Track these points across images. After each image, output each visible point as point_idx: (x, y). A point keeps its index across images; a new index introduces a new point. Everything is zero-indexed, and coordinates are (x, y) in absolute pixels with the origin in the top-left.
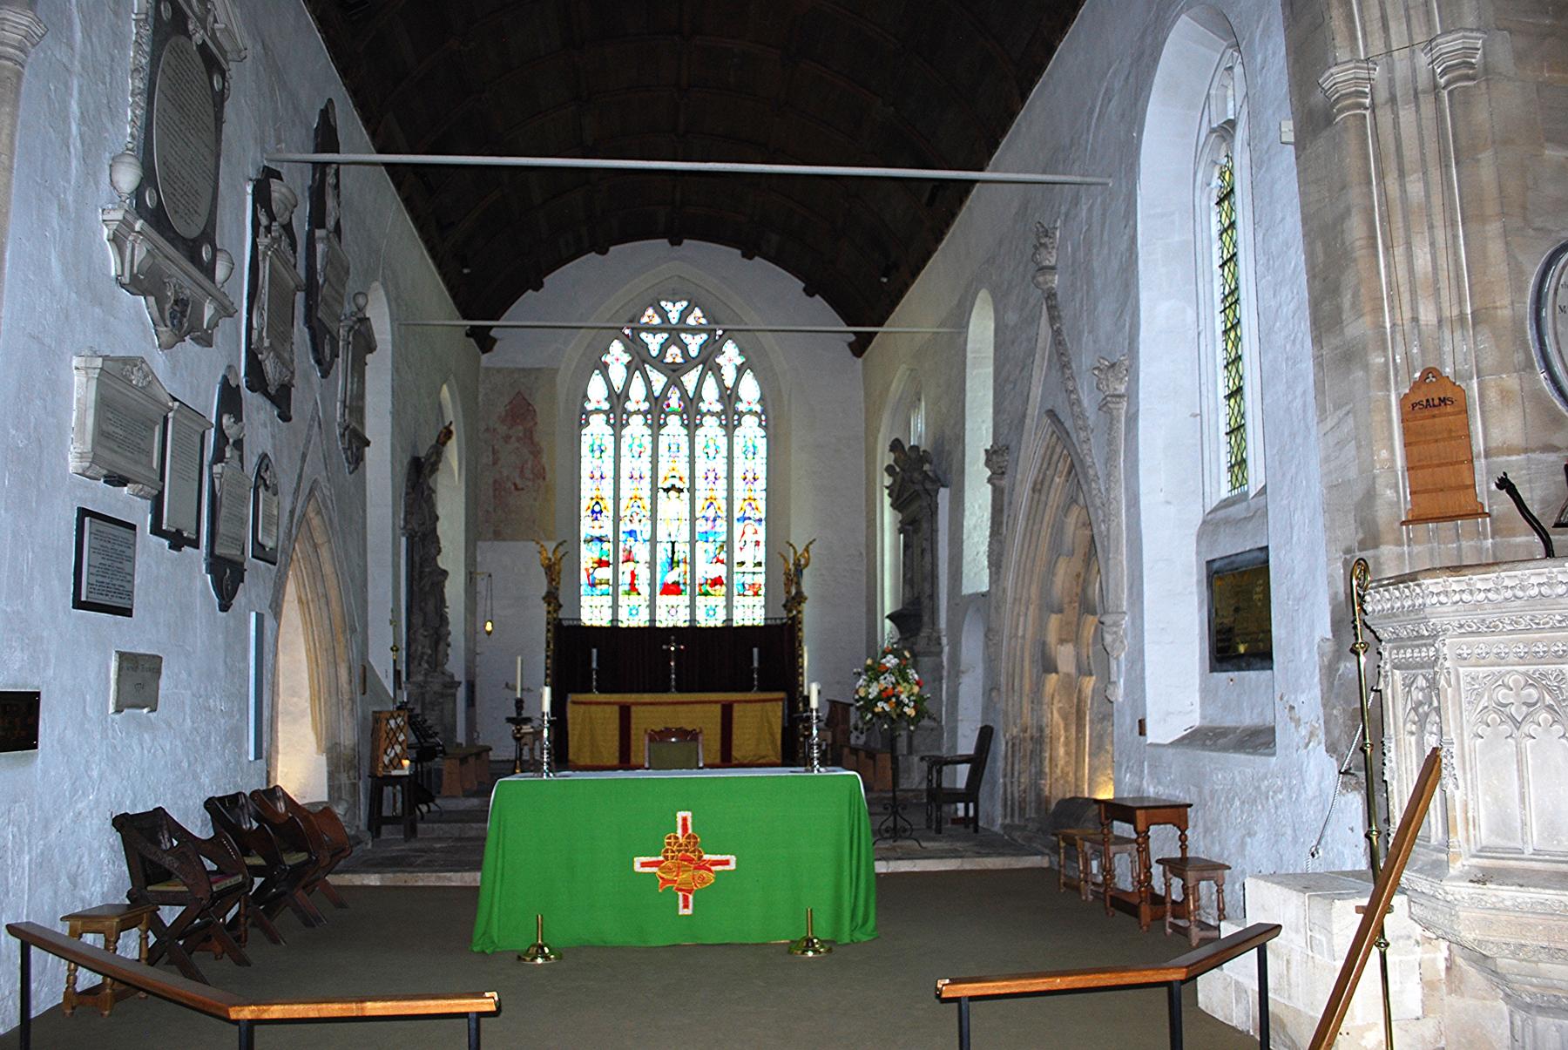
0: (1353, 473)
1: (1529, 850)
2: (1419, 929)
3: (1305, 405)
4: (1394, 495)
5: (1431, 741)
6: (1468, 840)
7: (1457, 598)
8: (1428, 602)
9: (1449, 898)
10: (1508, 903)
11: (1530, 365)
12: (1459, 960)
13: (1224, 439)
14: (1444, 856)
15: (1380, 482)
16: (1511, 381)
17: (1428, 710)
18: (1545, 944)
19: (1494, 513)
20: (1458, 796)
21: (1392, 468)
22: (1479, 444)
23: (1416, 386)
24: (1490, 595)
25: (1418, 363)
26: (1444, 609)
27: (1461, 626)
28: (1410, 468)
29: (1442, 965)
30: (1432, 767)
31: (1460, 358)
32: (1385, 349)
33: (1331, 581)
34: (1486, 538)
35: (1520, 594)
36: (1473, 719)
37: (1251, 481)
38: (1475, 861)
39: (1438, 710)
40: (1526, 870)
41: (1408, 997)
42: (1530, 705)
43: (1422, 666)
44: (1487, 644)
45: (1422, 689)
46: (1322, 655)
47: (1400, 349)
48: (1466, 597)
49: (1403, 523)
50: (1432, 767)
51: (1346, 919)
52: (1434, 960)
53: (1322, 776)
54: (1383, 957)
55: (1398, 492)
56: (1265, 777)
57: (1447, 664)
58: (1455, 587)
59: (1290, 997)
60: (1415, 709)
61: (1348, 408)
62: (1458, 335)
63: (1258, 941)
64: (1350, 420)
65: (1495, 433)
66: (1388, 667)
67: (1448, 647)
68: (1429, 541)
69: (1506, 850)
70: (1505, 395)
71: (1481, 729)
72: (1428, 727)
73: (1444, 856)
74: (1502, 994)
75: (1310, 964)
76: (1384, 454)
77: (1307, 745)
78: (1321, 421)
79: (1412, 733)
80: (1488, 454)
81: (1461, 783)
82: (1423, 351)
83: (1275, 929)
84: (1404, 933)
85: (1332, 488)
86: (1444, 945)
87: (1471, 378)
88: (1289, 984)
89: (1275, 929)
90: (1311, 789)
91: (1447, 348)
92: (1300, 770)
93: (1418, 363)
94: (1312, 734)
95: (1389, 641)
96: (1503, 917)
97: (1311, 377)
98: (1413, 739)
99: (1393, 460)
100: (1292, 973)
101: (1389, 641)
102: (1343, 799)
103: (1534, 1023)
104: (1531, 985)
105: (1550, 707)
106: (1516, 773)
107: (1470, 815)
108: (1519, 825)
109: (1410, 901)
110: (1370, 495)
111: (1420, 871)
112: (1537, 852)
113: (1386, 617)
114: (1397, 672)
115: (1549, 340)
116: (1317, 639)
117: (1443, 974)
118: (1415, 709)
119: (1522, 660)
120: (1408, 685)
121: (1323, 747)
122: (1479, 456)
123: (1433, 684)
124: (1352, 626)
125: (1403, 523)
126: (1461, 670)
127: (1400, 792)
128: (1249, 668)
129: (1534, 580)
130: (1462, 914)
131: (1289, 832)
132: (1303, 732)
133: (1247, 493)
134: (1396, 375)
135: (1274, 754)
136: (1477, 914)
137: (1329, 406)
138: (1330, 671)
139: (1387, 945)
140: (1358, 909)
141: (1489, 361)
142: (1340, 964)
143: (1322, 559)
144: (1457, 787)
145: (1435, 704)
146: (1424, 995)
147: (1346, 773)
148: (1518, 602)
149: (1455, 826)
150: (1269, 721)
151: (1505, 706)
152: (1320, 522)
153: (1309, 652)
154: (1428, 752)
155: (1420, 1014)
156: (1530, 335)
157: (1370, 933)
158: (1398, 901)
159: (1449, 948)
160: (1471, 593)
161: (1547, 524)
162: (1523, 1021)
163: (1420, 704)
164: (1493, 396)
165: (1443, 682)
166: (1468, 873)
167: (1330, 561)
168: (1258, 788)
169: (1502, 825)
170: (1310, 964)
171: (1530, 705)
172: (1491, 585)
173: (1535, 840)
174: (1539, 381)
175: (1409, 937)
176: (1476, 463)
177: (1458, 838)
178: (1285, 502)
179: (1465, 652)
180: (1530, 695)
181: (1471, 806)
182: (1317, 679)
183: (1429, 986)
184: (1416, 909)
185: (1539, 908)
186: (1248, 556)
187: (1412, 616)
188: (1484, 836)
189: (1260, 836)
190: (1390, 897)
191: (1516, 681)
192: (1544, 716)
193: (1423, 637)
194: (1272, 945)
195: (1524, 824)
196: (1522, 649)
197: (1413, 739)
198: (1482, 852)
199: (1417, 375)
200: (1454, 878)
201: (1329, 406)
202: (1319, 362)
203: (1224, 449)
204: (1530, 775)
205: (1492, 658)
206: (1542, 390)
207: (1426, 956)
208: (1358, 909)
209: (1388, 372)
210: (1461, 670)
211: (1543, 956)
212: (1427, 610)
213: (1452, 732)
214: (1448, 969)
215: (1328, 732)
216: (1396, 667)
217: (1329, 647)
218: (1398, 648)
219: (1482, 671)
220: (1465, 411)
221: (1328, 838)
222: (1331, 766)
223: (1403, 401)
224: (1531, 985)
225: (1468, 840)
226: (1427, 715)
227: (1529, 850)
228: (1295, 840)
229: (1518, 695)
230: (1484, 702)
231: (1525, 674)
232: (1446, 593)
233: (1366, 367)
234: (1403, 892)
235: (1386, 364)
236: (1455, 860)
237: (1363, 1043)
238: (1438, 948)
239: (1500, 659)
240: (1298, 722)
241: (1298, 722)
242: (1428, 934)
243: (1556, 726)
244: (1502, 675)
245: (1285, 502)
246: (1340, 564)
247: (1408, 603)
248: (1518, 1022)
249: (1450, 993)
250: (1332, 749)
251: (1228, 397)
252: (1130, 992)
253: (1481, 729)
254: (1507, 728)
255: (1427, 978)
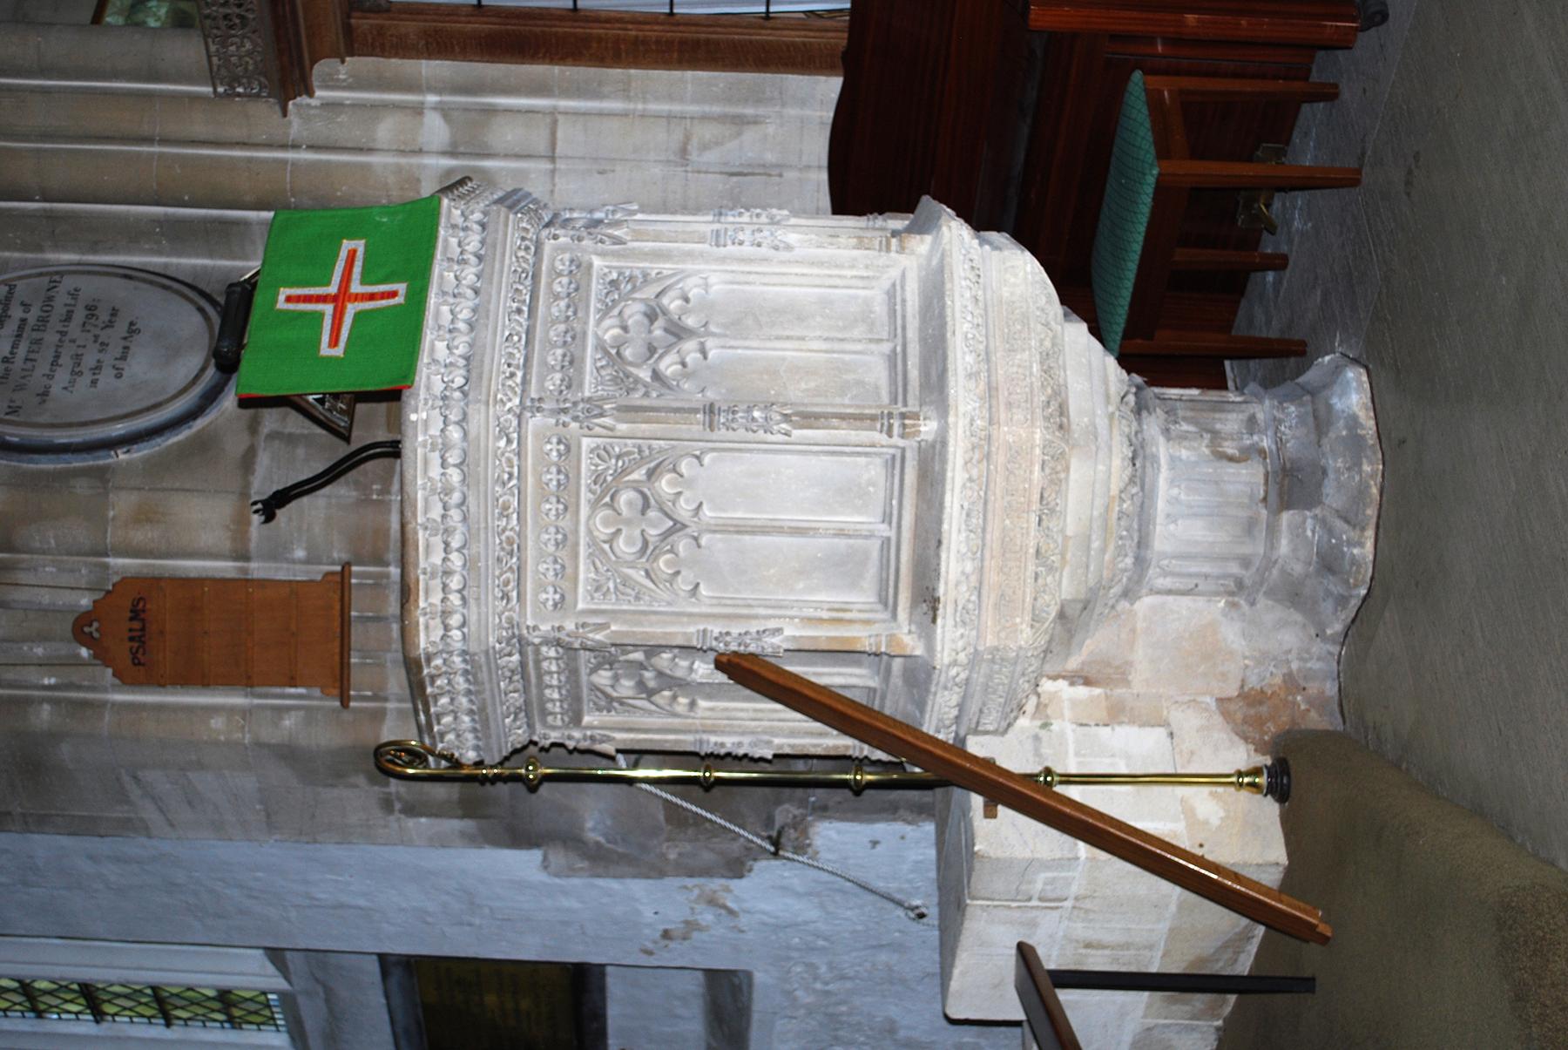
0: (247, 783)
1: (884, 530)
2: (1023, 722)
3: (118, 859)
4: (294, 713)
5: (704, 670)
6: (867, 622)
7: (455, 599)
8: (459, 646)
9: (962, 657)
10: (969, 567)
11: (101, 474)
12: (1073, 663)
13: (176, 1033)
14: (897, 664)
15: (268, 734)
16: (122, 503)
17: (644, 664)
18: (1034, 519)
19: (345, 557)
20: (793, 631)
21: (245, 712)
22: (224, 568)
23: (102, 655)
24: (455, 544)
25: (63, 649)
26: (473, 618)
27: (506, 596)
28: (244, 679)
29: (1082, 691)
30: (747, 672)
31: (65, 580)
32: (28, 701)
33: (441, 842)
34: (387, 576)
35: (456, 497)
36: (666, 596)
37: (262, 983)
38: (903, 614)
39: (653, 650)
40: (916, 536)
41: (1133, 746)
42: (646, 505)
43: (573, 673)
44: (541, 556)
45: (616, 678)
46: (571, 872)
47: (32, 675)
48: (455, 583)
49: (345, 703)
50: (747, 672)
51: (1006, 835)
52: (1074, 703)
53: (785, 890)
54: (1069, 779)
55: (289, 709)
56: (789, 994)
57: (570, 626)
58: (436, 598)
59: (1151, 947)
60: (650, 693)
61: (126, 779)
62: (23, 577)
63: (1045, 982)
64: (149, 776)
65: (207, 539)
66: (577, 734)
67: (540, 623)
68: (382, 666)
69: (884, 564)
70: (144, 516)
71: (683, 585)
72: (679, 673)
73: (897, 664)
74: (1124, 605)
75: (1088, 904)
76: (217, 723)
77: (731, 912)
78: (145, 829)
79: (693, 704)
80: (244, 556)
81: (772, 624)
82: (43, 638)
83: (1025, 953)
84: (1029, 745)
85: (271, 823)
86: (1047, 686)
87: (106, 566)
88: (1126, 946)
89: (1025, 953)
90: (807, 911)
91: (46, 597)
92: (777, 928)
93: (63, 649)
94: (712, 902)
95: (531, 726)
96: (992, 577)
97: (65, 841)
98: (703, 704)
99: (231, 710)
100: (1107, 938)
101: (531, 726)
102: (824, 855)
103: (1164, 555)
104: (1103, 550)
105: (651, 474)
106: (759, 539)
107: (825, 615)
108: (842, 543)
109: (976, 732)
110: (289, 754)
111: (921, 705)
112: (887, 518)
113: (485, 722)
114: (587, 719)
115: (61, 437)
116: (542, 877)
117: (1097, 691)
118: (650, 693)
119: (569, 509)
120: (609, 702)
121: (735, 884)
122: (245, 571)
123: (607, 656)
124: (511, 793)
125: (345, 703)
126: (581, 606)
127: (793, 733)
128: (600, 1016)
129: (435, 471)
130: (990, 641)
131: (883, 957)
132: (707, 917)
133: (283, 995)
134: (79, 688)
135: (749, 975)
136: (988, 618)
137: (119, 812)
138: (600, 859)
139: (1048, 771)
140: (990, 813)
141: (80, 533)
142: (1083, 849)
143: (401, 854)
144: (779, 631)
145: (638, 656)
146: (1132, 722)
147: (776, 843)
148: (471, 500)
149: (847, 639)
150: (693, 985)
151: (646, 543)
152: (333, 851)
153: (565, 892)
154: (721, 678)
155: (1161, 733)
156: (47, 464)
157: (1036, 797)
158: (977, 746)
159: (1055, 678)
160: (448, 573)
161: (343, 450)
162: (1165, 574)
163: (641, 685)
164: (140, 536)
165: (599, 637)
166: (920, 625)
167: (404, 841)
168: (810, 1011)
169: (843, 568)
170: (1088, 904)
171: (646, 505)
172: (437, 541)
173: (866, 519)
174: (129, 463)
175: (1037, 738)
176: (256, 575)
177: (863, 636)
178: (293, 914)
179: (550, 596)
180: (630, 503)
181: (810, 612)
182: (614, 884)
183: (1116, 714)
184: (989, 722)
185: (976, 521)
186: (397, 1000)
187: (484, 676)
188: (862, 597)
189: (893, 1011)
190: (974, 759)
191: (606, 523)
192: (665, 485)
193: (523, 664)
194: (1052, 959)
195: (841, 533)
196: (551, 506)
197: (703, 704)
198: (887, 601)
199: (84, 652)
200: (930, 648)
201: (119, 812)
202: (38, 822)
203: (198, 1033)
204: (762, 517)
205: (563, 554)
206: (146, 461)
207: (1067, 713)
208: (990, 813)
209: (71, 702)
210: (581, 606)
211: (1053, 524)
212: (473, 647)
213: (687, 631)
214: (1087, 682)
215: (707, 872)
216: (576, 720)
217: (558, 857)
218: (544, 713)
219: (584, 572)
220: (155, 583)
221: (891, 887)
222: (766, 872)
223: (126, 679)
224: (1103, 550)
225: (867, 622)
226: (660, 674)
227: (884, 530)
228: (897, 947)
229: (629, 522)
230: (639, 576)
231: (595, 505)
232: (445, 614)
233: (55, 736)
234: (963, 741)
235: (50, 700)
236: (900, 644)
237: (1215, 821)
238: (1054, 695)
239: (566, 541)
240: (691, 926)
241: (691, 926)
242: (1030, 706)
243: (684, 467)
244: (593, 542)
245: (293, 914)
246: (411, 823)
247: (461, 683)
248: (1167, 582)
249: (1126, 682)
250: (736, 868)
251: (99, 1016)
252: (1003, 1029)
253: (683, 585)
254: (683, 545)
255: (1102, 714)
